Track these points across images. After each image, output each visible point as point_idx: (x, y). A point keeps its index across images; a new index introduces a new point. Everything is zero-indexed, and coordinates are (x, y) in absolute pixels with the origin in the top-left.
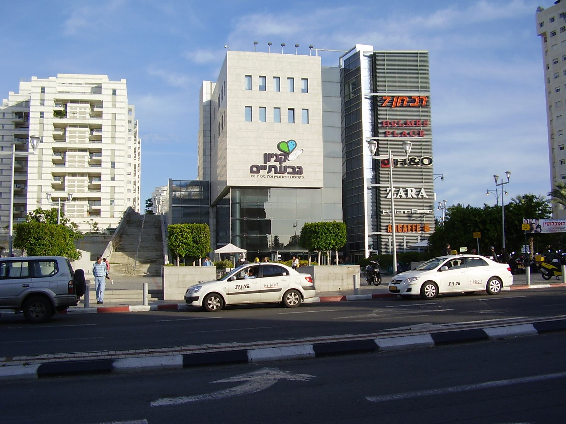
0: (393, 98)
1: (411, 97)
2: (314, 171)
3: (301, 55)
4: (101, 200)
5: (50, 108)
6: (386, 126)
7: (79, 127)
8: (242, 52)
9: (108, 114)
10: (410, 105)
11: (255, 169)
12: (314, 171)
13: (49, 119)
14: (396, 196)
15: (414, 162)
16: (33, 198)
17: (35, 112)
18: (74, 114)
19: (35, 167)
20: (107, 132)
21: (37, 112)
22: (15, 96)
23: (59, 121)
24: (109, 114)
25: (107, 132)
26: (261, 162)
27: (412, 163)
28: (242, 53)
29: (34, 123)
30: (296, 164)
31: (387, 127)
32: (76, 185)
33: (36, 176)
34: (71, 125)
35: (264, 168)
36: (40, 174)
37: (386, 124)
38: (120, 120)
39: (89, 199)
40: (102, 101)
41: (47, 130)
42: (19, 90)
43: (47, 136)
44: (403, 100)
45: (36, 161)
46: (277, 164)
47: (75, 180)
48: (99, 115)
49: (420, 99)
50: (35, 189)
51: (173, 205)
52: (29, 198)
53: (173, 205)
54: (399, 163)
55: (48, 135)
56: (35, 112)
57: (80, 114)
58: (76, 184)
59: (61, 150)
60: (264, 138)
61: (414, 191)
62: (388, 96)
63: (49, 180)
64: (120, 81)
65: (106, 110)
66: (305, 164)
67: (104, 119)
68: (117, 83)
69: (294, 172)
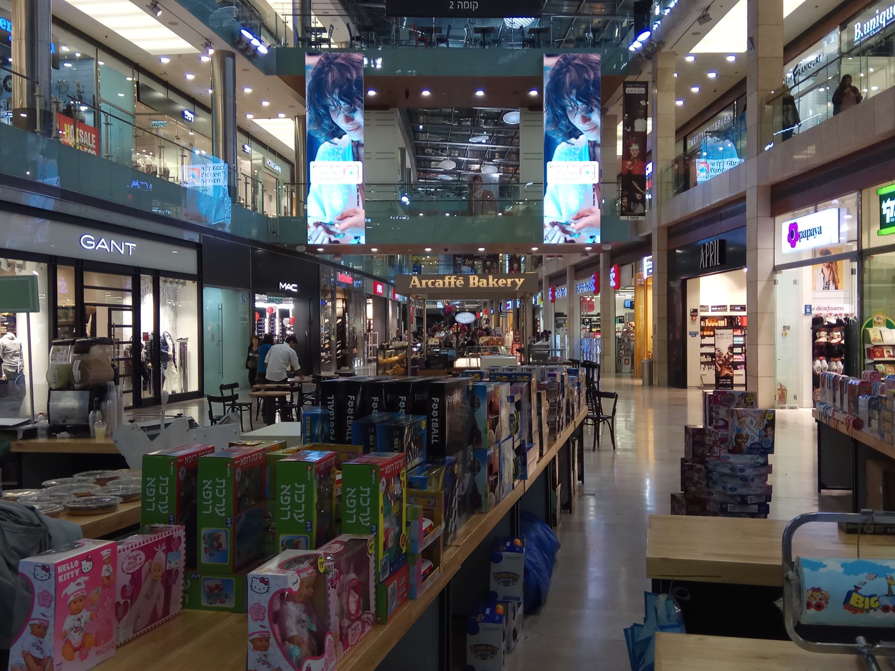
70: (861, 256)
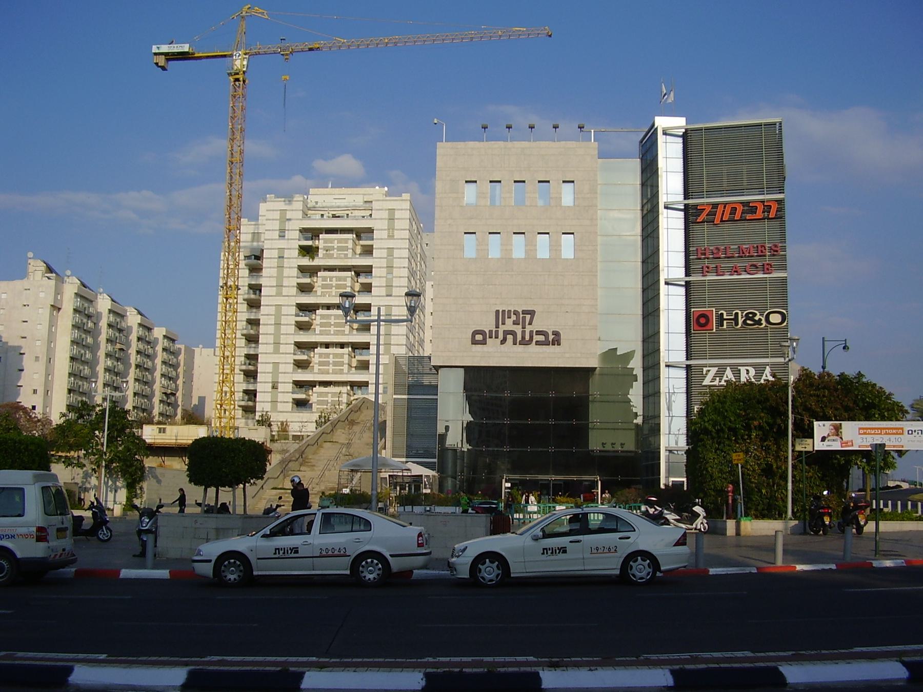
0: (715, 206)
1: (749, 202)
2: (582, 340)
3: (562, 142)
4: (369, 385)
5: (295, 241)
6: (703, 256)
7: (339, 271)
8: (462, 143)
9: (381, 249)
10: (747, 218)
11: (479, 337)
12: (582, 340)
13: (291, 260)
14: (720, 382)
15: (752, 319)
16: (265, 382)
17: (271, 249)
18: (327, 251)
19: (270, 334)
20: (380, 277)
21: (273, 249)
22: (249, 225)
23: (306, 261)
24: (384, 248)
25: (380, 277)
26: (488, 324)
27: (749, 322)
28: (461, 145)
29: (269, 266)
30: (550, 327)
31: (705, 258)
32: (331, 362)
33: (271, 348)
34: (325, 267)
35: (493, 335)
36: (277, 344)
37: (702, 254)
38: (400, 258)
39: (353, 385)
40: (373, 230)
41: (289, 277)
42: (258, 216)
43: (289, 287)
44: (734, 210)
45: (272, 325)
46: (518, 329)
47: (330, 354)
48: (368, 251)
49: (764, 206)
50: (270, 368)
51: (395, 396)
52: (261, 382)
53: (395, 396)
54: (725, 322)
55: (290, 285)
56: (271, 249)
57: (338, 251)
58: (331, 360)
59: (311, 307)
60: (495, 285)
61: (752, 372)
62: (708, 204)
63: (288, 355)
64: (401, 196)
65: (379, 242)
66: (567, 327)
67: (376, 258)
68: (396, 200)
69: (546, 343)
70: (669, 393)
